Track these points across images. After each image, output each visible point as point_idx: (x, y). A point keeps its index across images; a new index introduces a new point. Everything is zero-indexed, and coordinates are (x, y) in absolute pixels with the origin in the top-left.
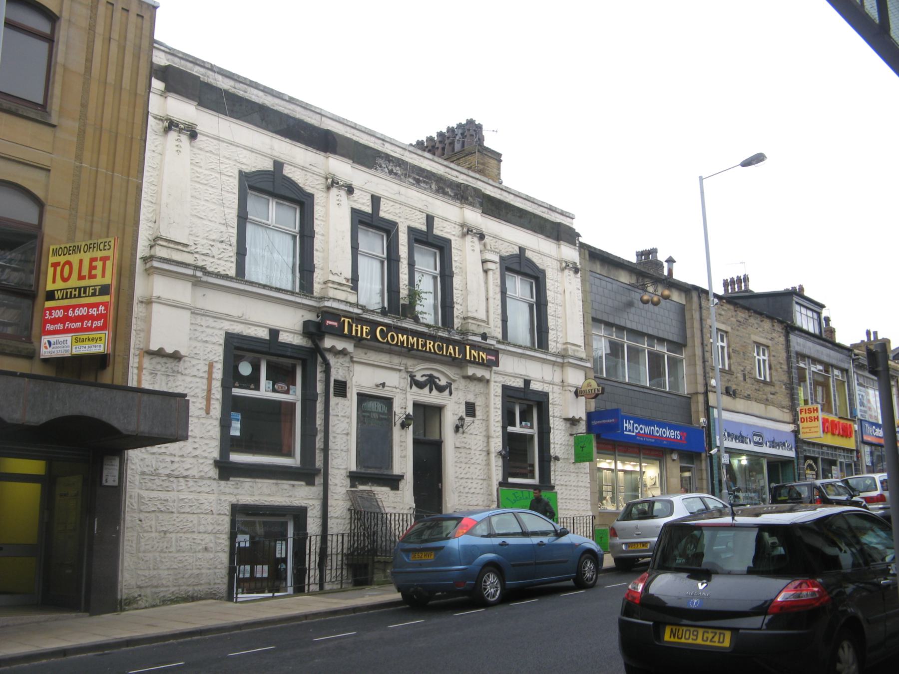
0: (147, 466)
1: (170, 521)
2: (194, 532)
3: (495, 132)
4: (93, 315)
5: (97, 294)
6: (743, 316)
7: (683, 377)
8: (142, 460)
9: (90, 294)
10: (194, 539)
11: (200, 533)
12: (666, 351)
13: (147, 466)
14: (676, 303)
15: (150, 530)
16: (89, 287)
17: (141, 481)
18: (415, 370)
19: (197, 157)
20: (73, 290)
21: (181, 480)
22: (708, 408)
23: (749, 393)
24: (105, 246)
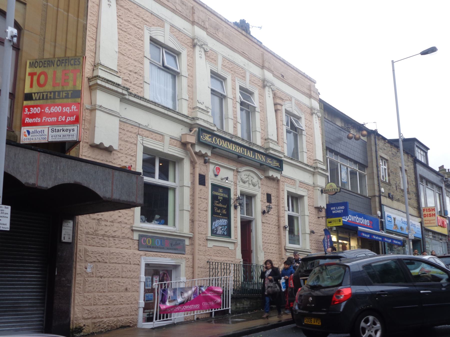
0: (90, 228)
1: (104, 269)
2: (119, 277)
3: (259, 28)
4: (66, 112)
5: (70, 97)
6: (395, 151)
7: (366, 186)
8: (87, 223)
9: (64, 97)
10: (119, 282)
11: (123, 277)
12: (358, 170)
13: (90, 228)
14: (362, 141)
15: (92, 276)
16: (63, 91)
17: (86, 239)
18: (242, 171)
19: (120, 11)
20: (49, 93)
21: (111, 239)
22: (381, 206)
23: (399, 198)
24: (75, 62)
